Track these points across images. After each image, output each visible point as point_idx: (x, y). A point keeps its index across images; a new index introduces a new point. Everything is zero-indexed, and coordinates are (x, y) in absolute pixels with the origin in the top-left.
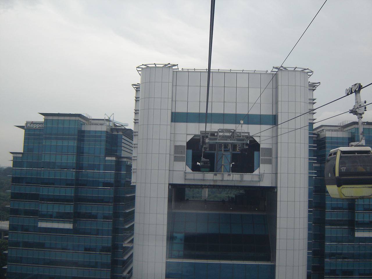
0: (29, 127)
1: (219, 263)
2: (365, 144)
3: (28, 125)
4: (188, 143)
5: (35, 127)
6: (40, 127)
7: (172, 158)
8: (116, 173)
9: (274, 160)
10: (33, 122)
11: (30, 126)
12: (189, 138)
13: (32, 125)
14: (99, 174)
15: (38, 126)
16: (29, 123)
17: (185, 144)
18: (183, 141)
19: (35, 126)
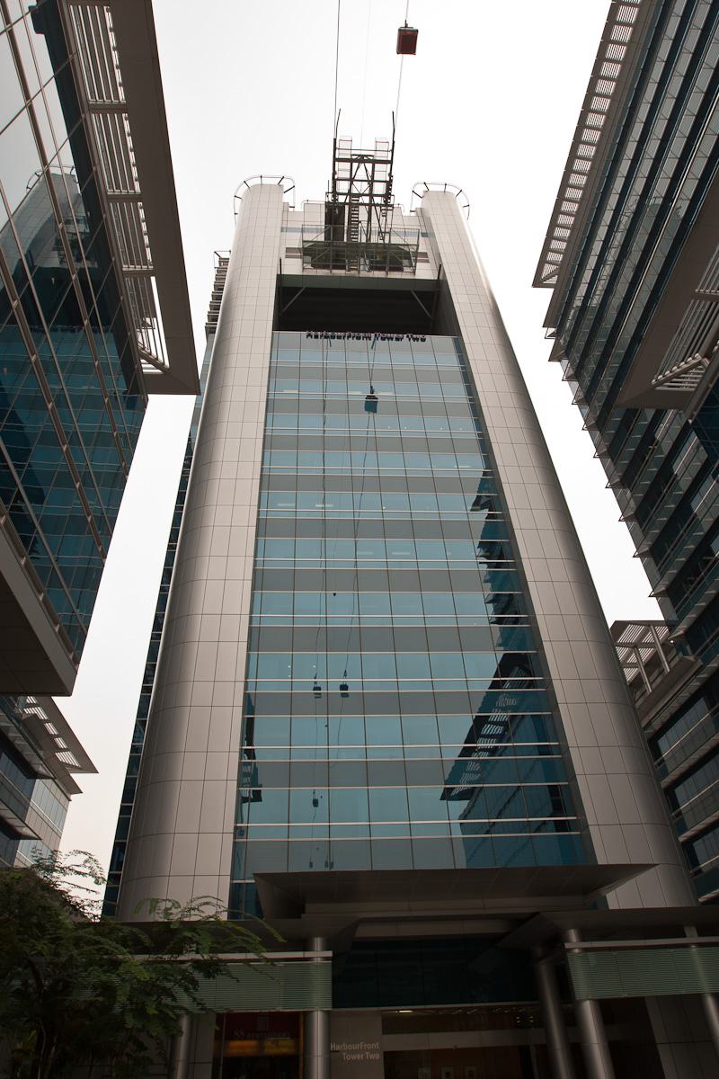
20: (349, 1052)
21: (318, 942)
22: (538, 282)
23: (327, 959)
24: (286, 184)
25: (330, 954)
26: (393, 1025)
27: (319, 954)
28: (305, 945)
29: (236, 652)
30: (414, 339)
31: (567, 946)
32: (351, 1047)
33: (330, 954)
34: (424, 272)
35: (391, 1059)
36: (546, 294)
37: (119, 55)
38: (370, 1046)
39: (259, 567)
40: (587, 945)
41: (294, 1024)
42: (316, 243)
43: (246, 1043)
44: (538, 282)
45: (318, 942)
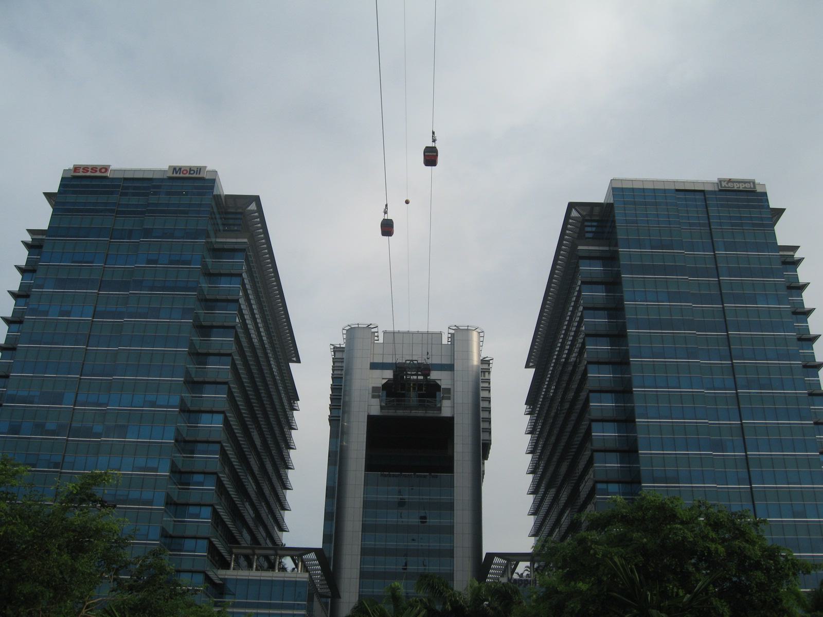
0: (725, 187)
1: (246, 579)
2: (443, 388)
3: (724, 184)
4: (383, 385)
5: (737, 188)
6: (745, 187)
7: (370, 396)
8: (618, 406)
9: (452, 397)
10: (730, 179)
11: (727, 186)
12: (384, 381)
13: (730, 185)
14: (154, 414)
15: (737, 185)
16: (724, 181)
17: (381, 386)
18: (380, 383)
19: (742, 185)
22: (527, 366)
34: (446, 412)
36: (532, 371)
42: (389, 380)
44: (527, 366)
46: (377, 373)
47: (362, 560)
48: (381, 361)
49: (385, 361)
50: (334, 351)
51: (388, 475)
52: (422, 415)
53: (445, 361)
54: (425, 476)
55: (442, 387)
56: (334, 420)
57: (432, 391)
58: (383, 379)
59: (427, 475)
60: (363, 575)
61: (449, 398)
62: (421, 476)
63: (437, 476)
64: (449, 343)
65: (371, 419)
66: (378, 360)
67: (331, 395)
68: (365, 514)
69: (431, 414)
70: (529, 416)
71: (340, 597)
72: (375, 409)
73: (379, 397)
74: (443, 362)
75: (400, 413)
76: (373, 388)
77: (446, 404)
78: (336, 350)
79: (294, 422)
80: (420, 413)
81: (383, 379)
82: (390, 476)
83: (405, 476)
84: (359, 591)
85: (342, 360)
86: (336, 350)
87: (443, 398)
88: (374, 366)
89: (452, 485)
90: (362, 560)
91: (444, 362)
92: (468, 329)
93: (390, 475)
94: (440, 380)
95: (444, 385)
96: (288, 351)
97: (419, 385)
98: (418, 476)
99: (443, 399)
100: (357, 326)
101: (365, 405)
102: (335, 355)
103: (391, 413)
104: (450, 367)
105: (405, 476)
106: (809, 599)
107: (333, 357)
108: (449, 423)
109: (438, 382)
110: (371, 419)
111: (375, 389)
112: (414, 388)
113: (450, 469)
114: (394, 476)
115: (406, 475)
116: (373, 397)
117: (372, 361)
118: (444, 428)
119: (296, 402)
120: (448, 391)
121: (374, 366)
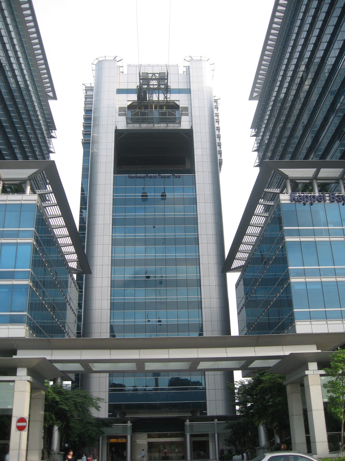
2: (181, 107)
7: (117, 114)
9: (190, 114)
20: (139, 442)
21: (129, 422)
22: (251, 98)
23: (131, 425)
24: (118, 59)
25: (131, 424)
26: (149, 436)
27: (129, 424)
28: (126, 423)
29: (106, 313)
30: (176, 177)
31: (307, 372)
32: (139, 441)
33: (131, 424)
34: (185, 124)
35: (149, 443)
36: (255, 103)
37: (70, 238)
38: (144, 441)
39: (113, 279)
40: (190, 423)
41: (125, 437)
42: (134, 102)
43: (114, 440)
44: (251, 98)
45: (129, 422)
46: (124, 96)
47: (113, 292)
48: (126, 88)
49: (129, 88)
50: (86, 90)
51: (135, 176)
52: (164, 128)
53: (183, 86)
54: (168, 177)
55: (180, 106)
56: (86, 144)
57: (171, 109)
58: (128, 101)
59: (170, 176)
60: (114, 263)
61: (187, 115)
62: (165, 177)
63: (179, 177)
64: (185, 73)
65: (118, 133)
66: (124, 87)
67: (83, 123)
68: (114, 210)
69: (171, 126)
70: (255, 138)
71: (91, 273)
72: (122, 124)
73: (125, 115)
74: (180, 88)
75: (144, 126)
76: (120, 108)
77: (184, 119)
78: (88, 89)
79: (51, 146)
80: (162, 126)
81: (128, 101)
82: (137, 177)
83: (151, 177)
84: (111, 299)
85: (91, 97)
86: (88, 89)
87: (182, 115)
88: (120, 91)
89: (194, 183)
90: (113, 292)
91: (181, 87)
92: (201, 60)
93: (137, 176)
94: (179, 101)
95: (182, 104)
96: (45, 90)
97: (160, 105)
98: (162, 177)
99: (182, 115)
100: (104, 59)
101: (112, 121)
102: (86, 93)
103: (136, 126)
104: (188, 91)
105: (151, 177)
106: (50, 402)
107: (85, 94)
108: (189, 134)
109: (177, 103)
110: (118, 133)
111: (121, 109)
112: (156, 108)
113: (192, 171)
114: (140, 177)
115: (151, 176)
116: (120, 115)
117: (118, 88)
118: (186, 138)
119: (53, 131)
120: (186, 109)
121: (120, 91)
